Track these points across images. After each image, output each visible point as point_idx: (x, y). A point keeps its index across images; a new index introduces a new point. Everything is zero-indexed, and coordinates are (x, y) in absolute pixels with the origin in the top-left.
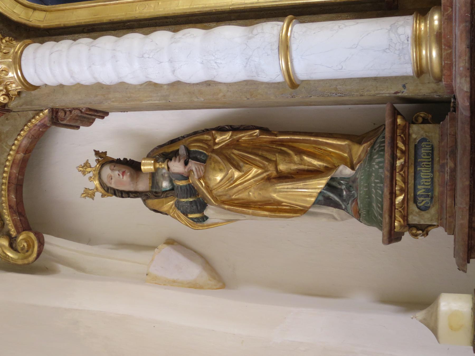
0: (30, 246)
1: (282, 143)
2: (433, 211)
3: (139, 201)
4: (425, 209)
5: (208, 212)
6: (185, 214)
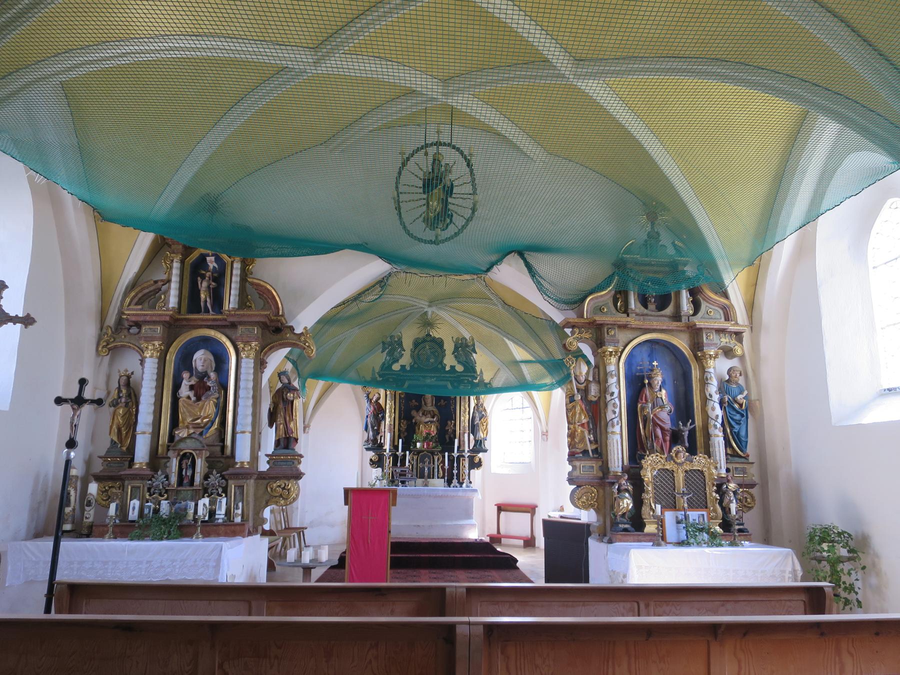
0: (105, 352)
1: (130, 428)
2: (106, 467)
3: (118, 386)
4: (107, 465)
5: (112, 409)
6: (112, 402)
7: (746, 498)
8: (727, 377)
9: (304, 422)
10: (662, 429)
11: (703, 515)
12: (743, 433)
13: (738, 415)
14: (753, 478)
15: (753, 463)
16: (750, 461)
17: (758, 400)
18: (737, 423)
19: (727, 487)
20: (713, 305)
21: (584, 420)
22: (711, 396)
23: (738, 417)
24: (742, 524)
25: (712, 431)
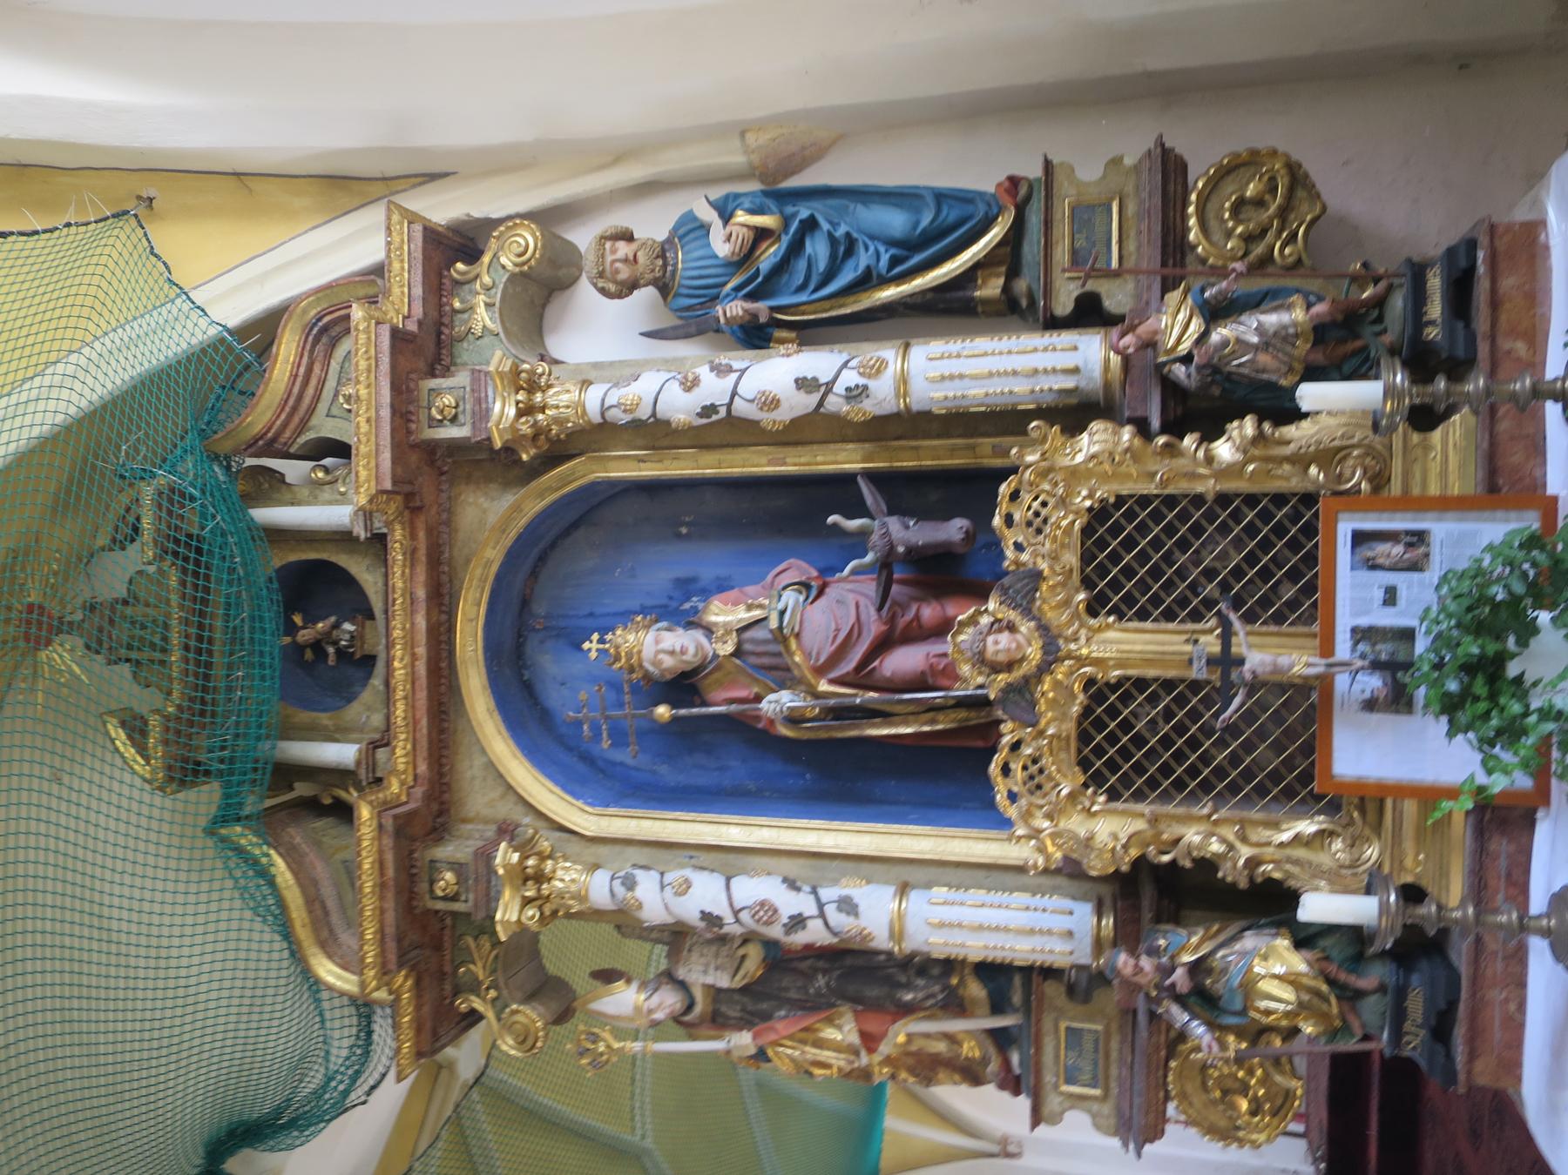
7: (1239, 206)
8: (647, 294)
9: (992, 1155)
10: (883, 645)
11: (1359, 538)
12: (895, 221)
13: (809, 248)
14: (1128, 161)
15: (1048, 166)
16: (1034, 171)
17: (743, 134)
18: (850, 251)
19: (1187, 359)
20: (322, 383)
21: (843, 1031)
22: (708, 410)
23: (817, 249)
24: (1418, 273)
25: (883, 396)
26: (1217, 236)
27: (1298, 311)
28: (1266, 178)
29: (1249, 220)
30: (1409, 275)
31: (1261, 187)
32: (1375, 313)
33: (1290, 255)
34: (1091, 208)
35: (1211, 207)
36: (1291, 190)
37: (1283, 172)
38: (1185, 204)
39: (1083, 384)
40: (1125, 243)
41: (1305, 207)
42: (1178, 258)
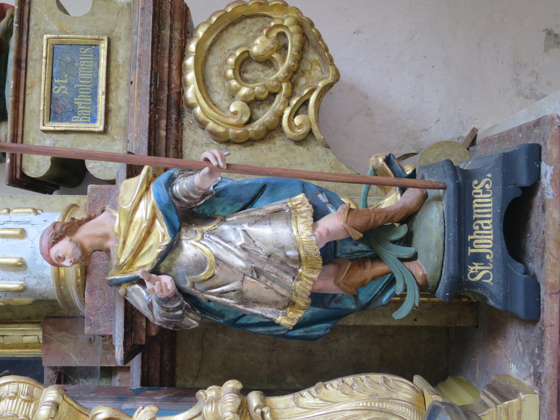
26: (219, 97)
27: (301, 227)
28: (274, 34)
29: (255, 81)
30: (451, 185)
31: (269, 43)
32: (403, 231)
33: (300, 126)
34: (74, 46)
35: (214, 61)
36: (302, 51)
37: (292, 29)
38: (183, 56)
39: (32, 283)
40: (113, 96)
41: (316, 72)
42: (174, 116)
